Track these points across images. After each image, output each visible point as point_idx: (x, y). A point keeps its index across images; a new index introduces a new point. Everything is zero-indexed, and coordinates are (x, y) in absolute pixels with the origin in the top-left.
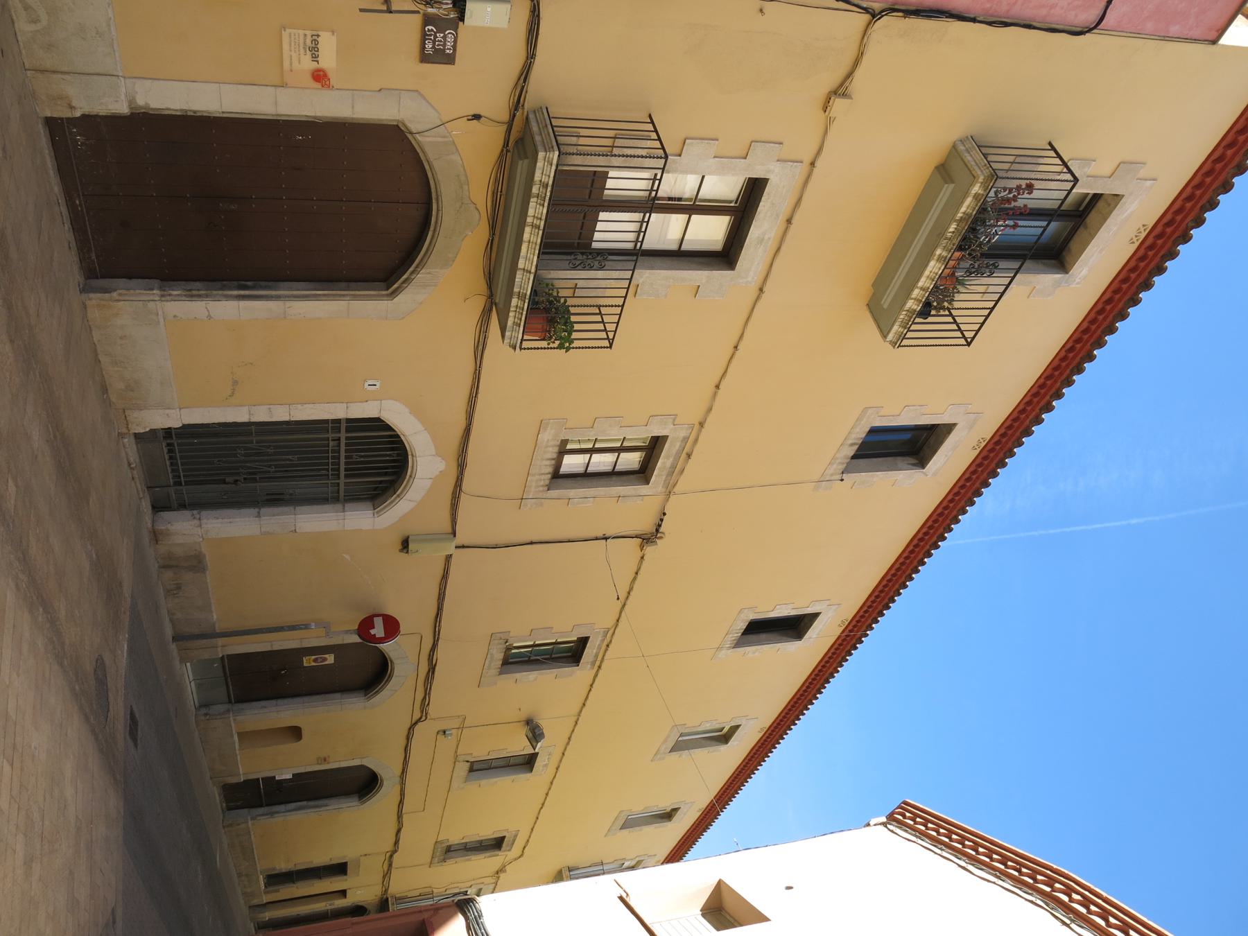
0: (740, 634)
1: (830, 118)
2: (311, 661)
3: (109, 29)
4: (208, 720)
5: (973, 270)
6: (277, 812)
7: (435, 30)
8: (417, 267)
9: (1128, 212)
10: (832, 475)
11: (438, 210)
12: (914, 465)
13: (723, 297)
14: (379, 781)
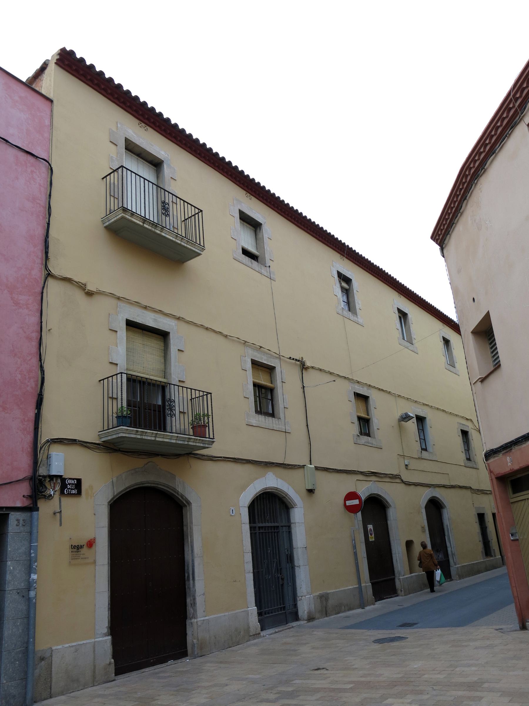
0: (350, 313)
1: (97, 291)
2: (372, 537)
3: (74, 646)
5: (166, 213)
7: (66, 489)
8: (175, 492)
9: (133, 134)
10: (267, 272)
12: (260, 230)
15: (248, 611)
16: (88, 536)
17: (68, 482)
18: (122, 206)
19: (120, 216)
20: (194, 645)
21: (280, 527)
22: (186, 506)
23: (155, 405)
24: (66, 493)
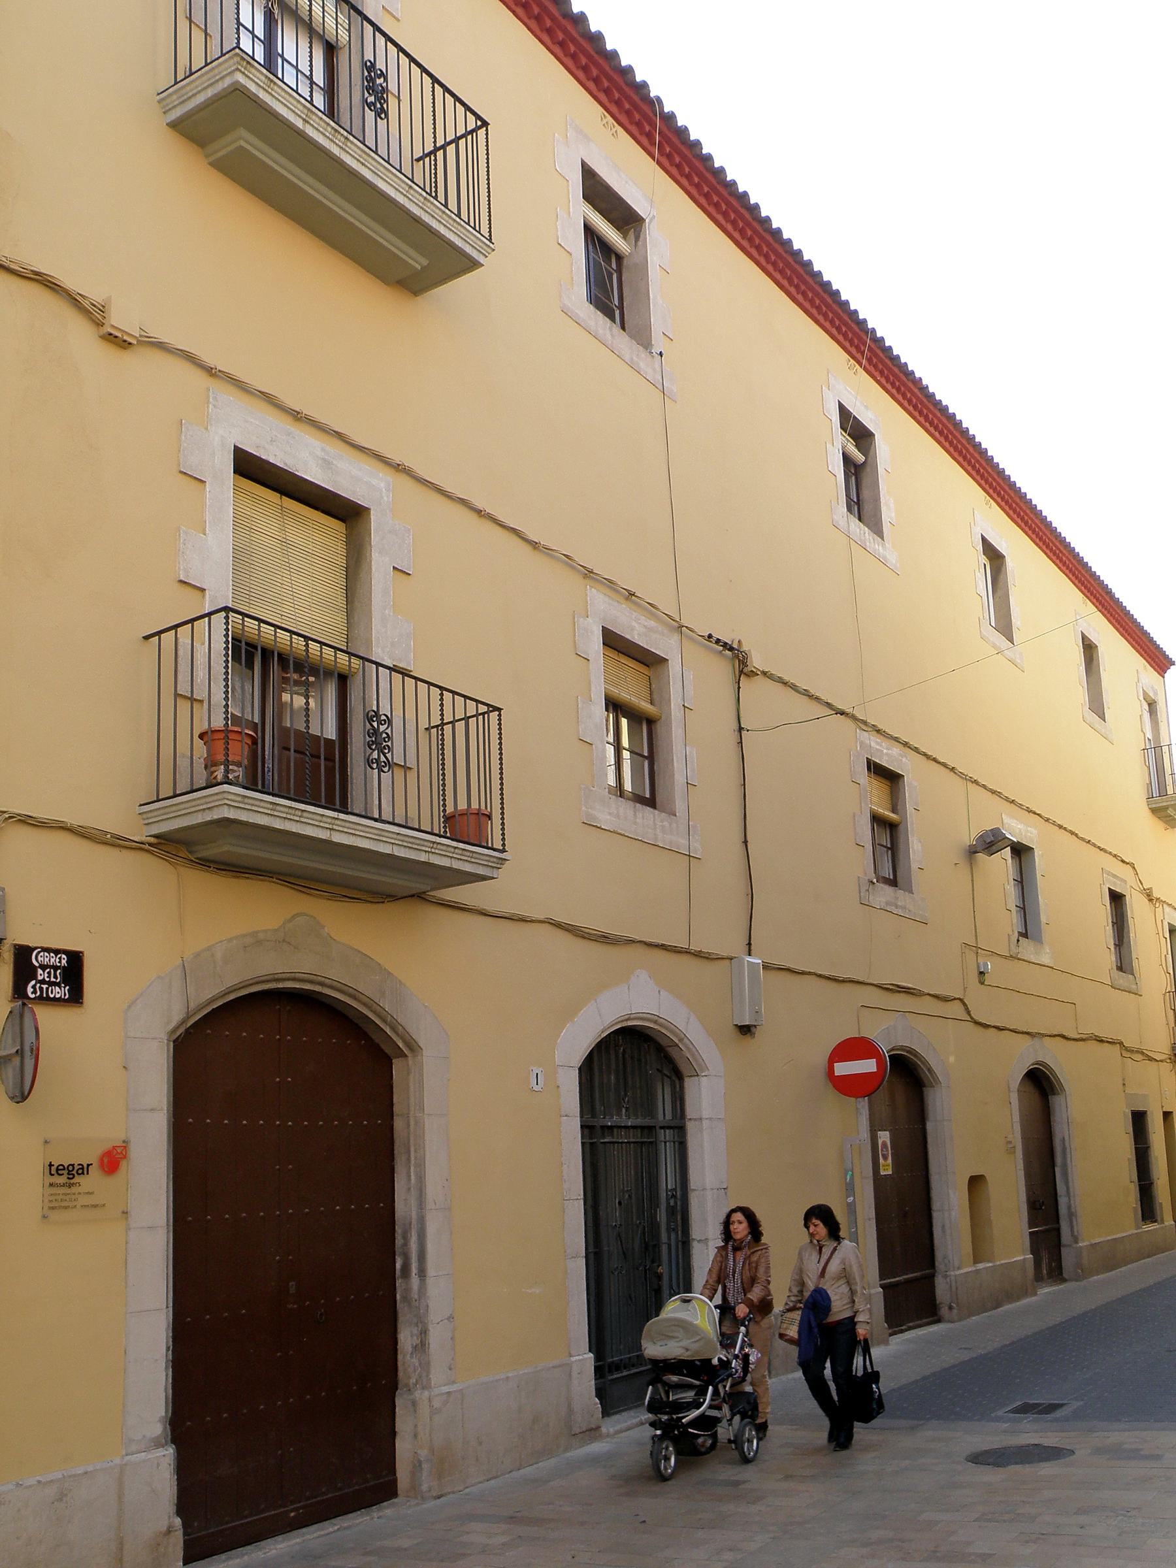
1: (141, 336)
4: (958, 1305)
6: (1069, 1207)
10: (654, 370)
11: (294, 979)
13: (409, 530)
14: (1036, 1066)
15: (570, 1365)
16: (108, 1133)
17: (40, 959)
18: (235, 45)
19: (227, 82)
20: (420, 1465)
21: (657, 1128)
22: (406, 1056)
23: (317, 739)
24: (33, 996)
